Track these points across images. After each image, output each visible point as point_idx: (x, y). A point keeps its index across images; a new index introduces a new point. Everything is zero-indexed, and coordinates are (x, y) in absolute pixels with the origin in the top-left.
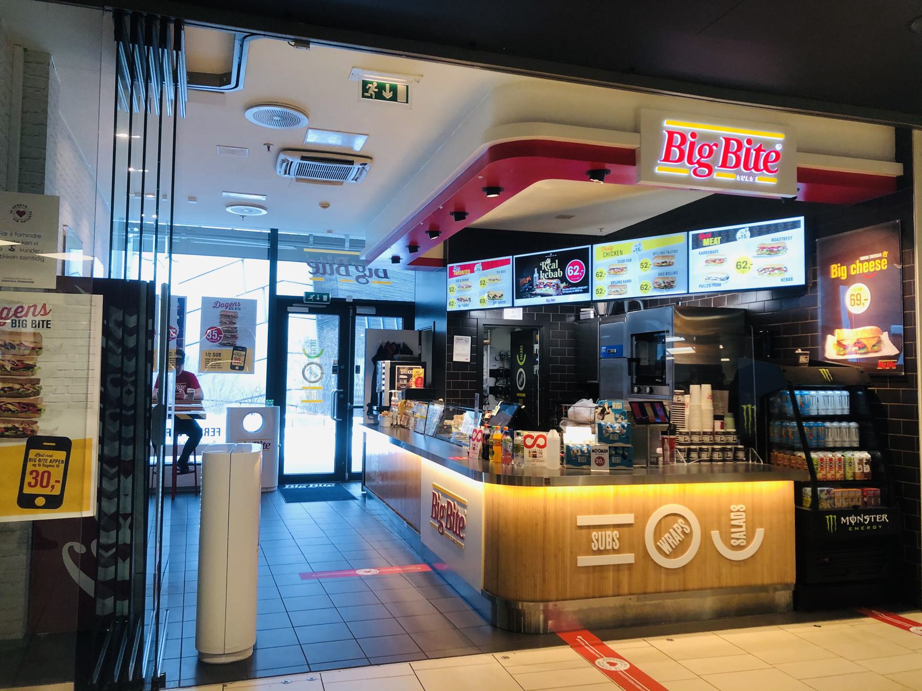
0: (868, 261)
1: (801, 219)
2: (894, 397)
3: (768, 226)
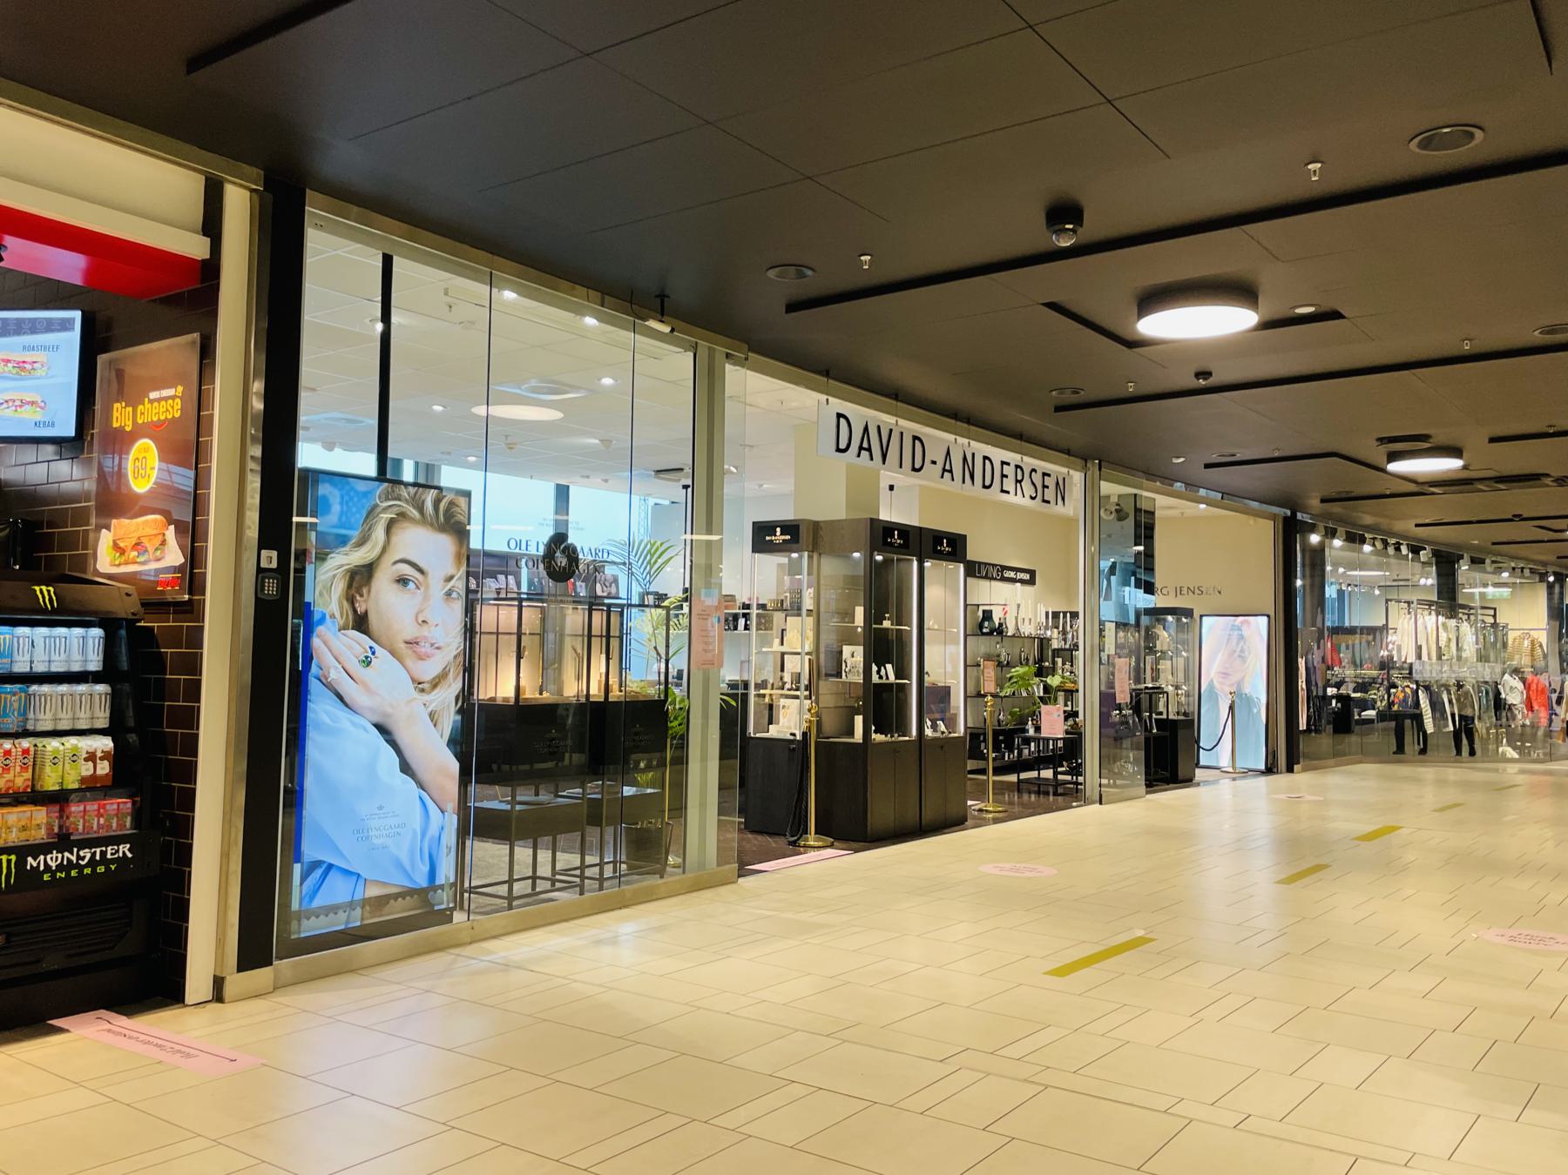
0: (159, 400)
1: (77, 315)
2: (175, 637)
3: (19, 321)
